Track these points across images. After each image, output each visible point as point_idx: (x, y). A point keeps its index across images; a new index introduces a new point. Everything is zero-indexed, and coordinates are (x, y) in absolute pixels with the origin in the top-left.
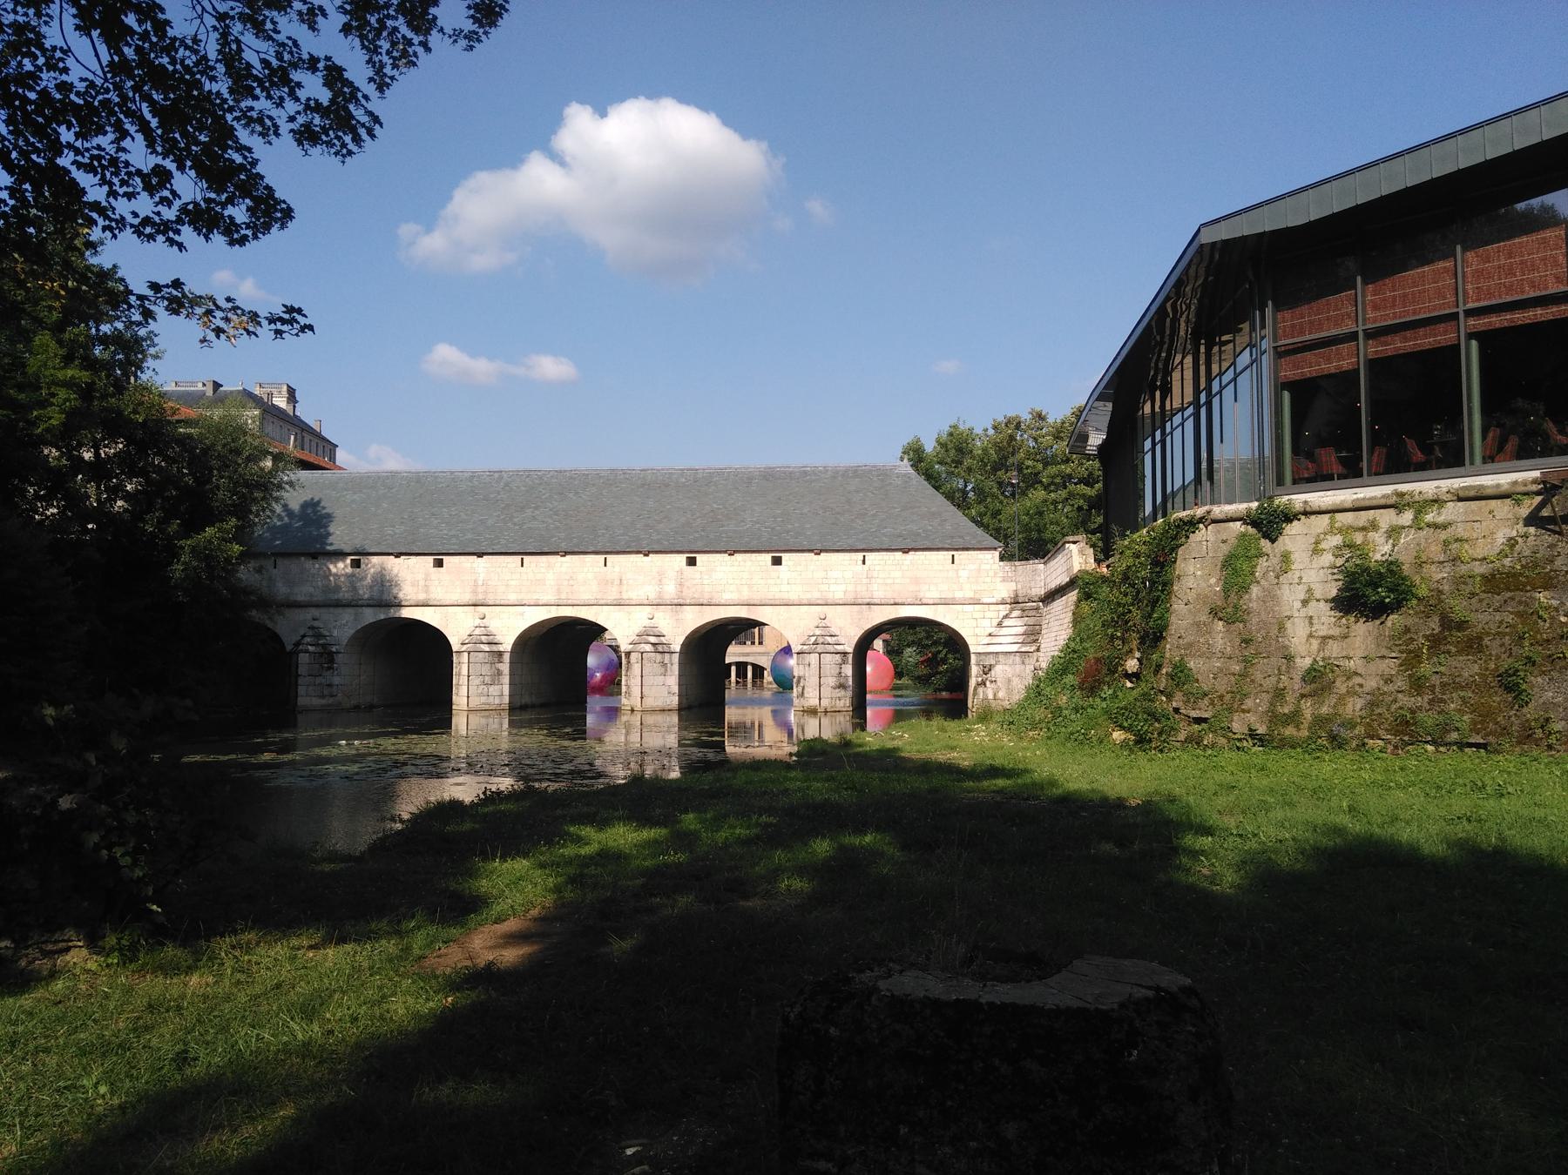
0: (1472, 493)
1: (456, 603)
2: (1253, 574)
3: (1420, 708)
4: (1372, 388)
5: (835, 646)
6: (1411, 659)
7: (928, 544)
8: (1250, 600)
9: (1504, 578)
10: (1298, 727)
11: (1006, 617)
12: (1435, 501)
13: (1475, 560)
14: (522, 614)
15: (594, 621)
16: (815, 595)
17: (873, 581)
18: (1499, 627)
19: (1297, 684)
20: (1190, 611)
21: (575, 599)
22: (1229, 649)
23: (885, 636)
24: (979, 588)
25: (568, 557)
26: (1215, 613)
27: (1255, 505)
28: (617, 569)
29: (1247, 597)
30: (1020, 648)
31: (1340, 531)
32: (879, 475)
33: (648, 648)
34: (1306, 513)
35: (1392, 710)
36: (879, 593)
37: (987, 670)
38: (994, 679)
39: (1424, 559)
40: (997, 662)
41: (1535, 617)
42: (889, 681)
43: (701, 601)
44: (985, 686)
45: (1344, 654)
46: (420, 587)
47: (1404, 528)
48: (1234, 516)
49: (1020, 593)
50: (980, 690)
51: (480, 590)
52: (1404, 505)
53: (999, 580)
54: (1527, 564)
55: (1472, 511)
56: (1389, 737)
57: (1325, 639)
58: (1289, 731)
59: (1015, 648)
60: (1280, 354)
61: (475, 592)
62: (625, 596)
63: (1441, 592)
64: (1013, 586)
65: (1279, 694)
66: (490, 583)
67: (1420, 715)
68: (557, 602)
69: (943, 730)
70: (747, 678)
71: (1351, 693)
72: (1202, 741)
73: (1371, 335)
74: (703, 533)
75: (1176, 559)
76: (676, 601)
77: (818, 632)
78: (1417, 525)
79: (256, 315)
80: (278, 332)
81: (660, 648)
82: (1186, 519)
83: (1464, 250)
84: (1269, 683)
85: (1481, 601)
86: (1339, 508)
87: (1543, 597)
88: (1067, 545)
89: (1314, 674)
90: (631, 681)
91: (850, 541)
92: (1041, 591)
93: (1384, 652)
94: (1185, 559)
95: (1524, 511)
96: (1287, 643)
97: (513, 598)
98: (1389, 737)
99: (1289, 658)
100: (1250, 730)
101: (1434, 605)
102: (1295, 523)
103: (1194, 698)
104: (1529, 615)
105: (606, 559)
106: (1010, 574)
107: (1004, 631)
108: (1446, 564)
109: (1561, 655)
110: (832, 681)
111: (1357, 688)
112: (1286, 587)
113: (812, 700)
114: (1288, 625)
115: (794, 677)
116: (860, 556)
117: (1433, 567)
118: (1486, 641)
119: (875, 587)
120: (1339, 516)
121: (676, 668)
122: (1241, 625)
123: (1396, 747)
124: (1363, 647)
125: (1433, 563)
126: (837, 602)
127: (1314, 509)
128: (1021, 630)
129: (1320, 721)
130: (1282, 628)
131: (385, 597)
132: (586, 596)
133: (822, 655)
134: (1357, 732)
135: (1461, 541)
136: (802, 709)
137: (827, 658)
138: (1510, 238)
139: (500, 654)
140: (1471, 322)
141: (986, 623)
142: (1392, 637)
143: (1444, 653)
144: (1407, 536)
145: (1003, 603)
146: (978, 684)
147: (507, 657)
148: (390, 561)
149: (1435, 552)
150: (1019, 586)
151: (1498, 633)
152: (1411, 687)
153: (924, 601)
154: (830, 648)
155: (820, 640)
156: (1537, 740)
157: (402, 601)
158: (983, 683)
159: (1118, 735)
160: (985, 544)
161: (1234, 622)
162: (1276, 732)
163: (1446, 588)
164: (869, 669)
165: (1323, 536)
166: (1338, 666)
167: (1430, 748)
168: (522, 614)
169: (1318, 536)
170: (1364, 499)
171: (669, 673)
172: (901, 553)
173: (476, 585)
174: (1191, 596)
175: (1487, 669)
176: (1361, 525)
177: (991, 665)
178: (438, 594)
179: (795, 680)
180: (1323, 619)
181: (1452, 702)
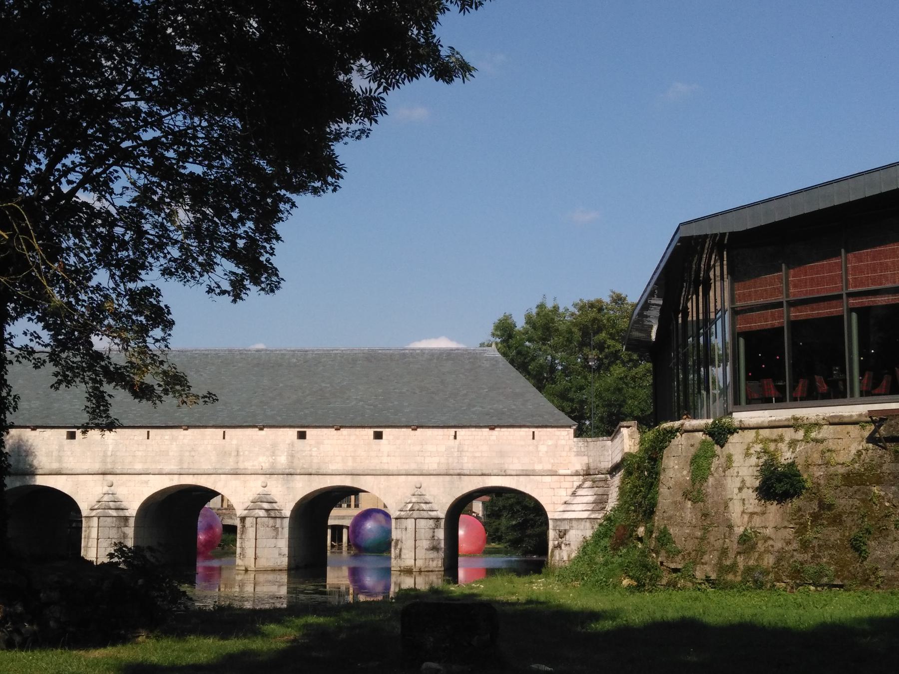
0: (837, 420)
1: (86, 472)
2: (709, 469)
3: (806, 561)
4: (793, 344)
5: (430, 512)
6: (801, 529)
7: (512, 422)
8: (707, 486)
9: (855, 477)
10: (735, 574)
11: (579, 487)
12: (817, 424)
13: (838, 464)
14: (147, 482)
15: (213, 489)
16: (412, 467)
17: (464, 454)
18: (851, 508)
19: (735, 546)
20: (671, 494)
21: (195, 468)
22: (694, 520)
23: (486, 498)
24: (556, 461)
25: (190, 431)
26: (686, 495)
27: (710, 421)
28: (234, 442)
29: (706, 484)
30: (590, 515)
31: (761, 441)
32: (469, 359)
33: (262, 513)
34: (743, 429)
35: (791, 562)
36: (468, 465)
37: (562, 534)
38: (568, 543)
39: (810, 462)
40: (571, 528)
41: (871, 503)
42: (480, 543)
43: (310, 471)
44: (561, 549)
45: (763, 525)
46: (54, 457)
47: (798, 441)
48: (699, 428)
49: (592, 466)
50: (557, 552)
51: (109, 460)
52: (798, 426)
53: (573, 454)
54: (868, 467)
55: (838, 432)
56: (788, 581)
57: (752, 514)
58: (730, 577)
59: (585, 515)
60: (735, 312)
61: (104, 462)
62: (241, 466)
63: (819, 484)
64: (585, 460)
65: (724, 552)
66: (118, 454)
67: (806, 566)
68: (179, 471)
69: (511, 582)
70: (342, 541)
71: (767, 551)
72: (677, 585)
73: (792, 304)
74: (312, 410)
75: (662, 456)
76: (287, 471)
77: (414, 500)
78: (806, 439)
79: (198, 396)
80: (205, 402)
81: (273, 514)
82: (668, 429)
83: (847, 252)
84: (718, 544)
85: (841, 491)
86: (761, 426)
87: (875, 489)
88: (622, 429)
89: (745, 538)
90: (246, 544)
91: (444, 418)
92: (609, 465)
93: (786, 524)
94: (668, 457)
95: (866, 434)
96: (729, 516)
97: (138, 467)
98: (788, 581)
99: (730, 527)
100: (707, 577)
101: (815, 493)
102: (735, 434)
103: (673, 554)
104: (867, 501)
105: (224, 432)
106: (583, 449)
107: (578, 500)
108: (822, 466)
109: (885, 528)
110: (425, 544)
111: (770, 548)
112: (729, 479)
113: (408, 561)
114: (730, 504)
115: (393, 540)
116: (452, 431)
117: (815, 468)
118: (844, 517)
119: (466, 459)
120: (761, 431)
121: (286, 532)
122: (702, 504)
123: (792, 588)
124: (774, 520)
125: (815, 465)
126: (431, 472)
127: (746, 426)
128: (591, 499)
129: (749, 570)
130: (726, 507)
131: (21, 466)
132: (206, 466)
133: (417, 520)
134: (770, 577)
135: (831, 451)
136: (399, 569)
137: (422, 523)
138: (874, 246)
139: (126, 519)
140: (851, 301)
141: (563, 493)
142: (791, 514)
143: (820, 525)
144: (800, 446)
145: (577, 474)
146: (555, 547)
147: (132, 522)
148: (28, 434)
149: (816, 457)
150: (591, 461)
151: (851, 513)
152: (801, 548)
153: (509, 472)
154: (425, 514)
155: (416, 507)
156: (871, 582)
157: (36, 469)
158: (559, 546)
159: (626, 582)
160: (561, 423)
161: (698, 502)
162: (722, 578)
163: (822, 482)
164: (461, 532)
165: (751, 444)
166: (760, 533)
167: (812, 588)
168: (147, 482)
169: (749, 445)
170: (775, 421)
171: (280, 536)
172: (488, 430)
173: (105, 456)
174: (671, 483)
175: (844, 535)
176: (774, 438)
177: (565, 530)
178: (70, 463)
179: (393, 544)
180: (751, 501)
181: (825, 557)
